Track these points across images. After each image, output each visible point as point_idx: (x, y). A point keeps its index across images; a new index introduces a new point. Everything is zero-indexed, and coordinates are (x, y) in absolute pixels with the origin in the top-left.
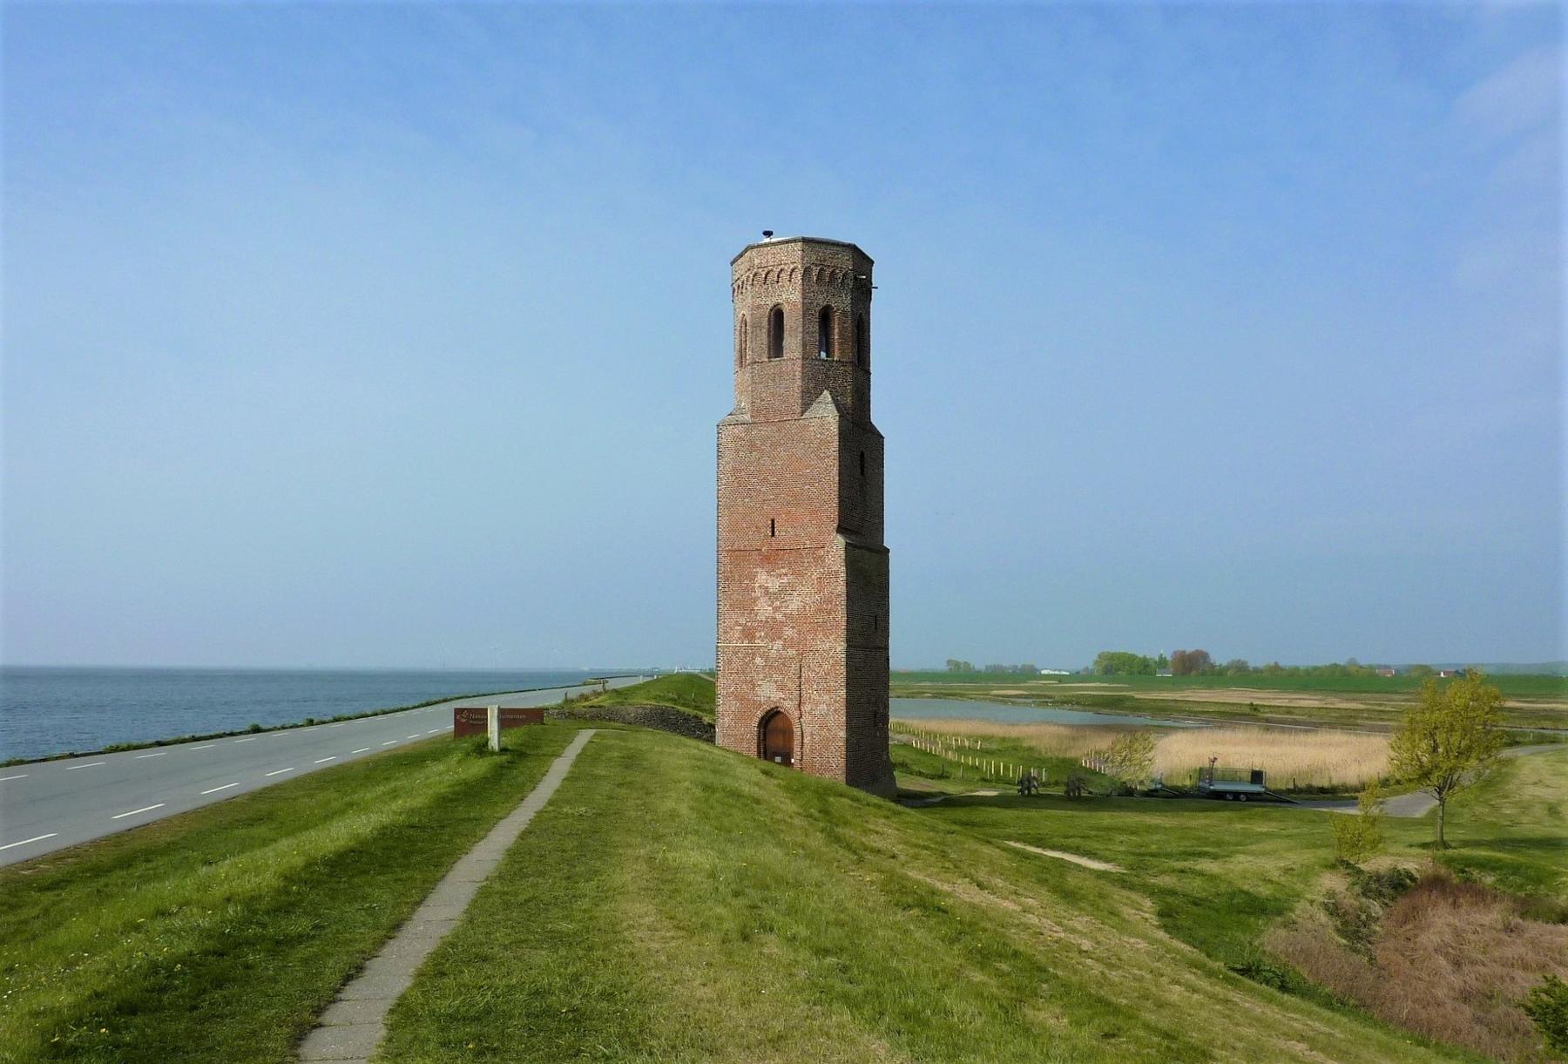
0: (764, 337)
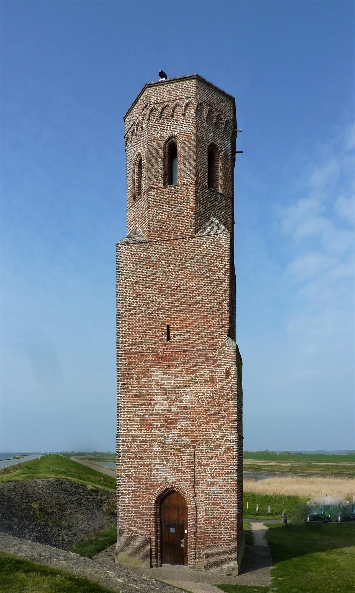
0: (159, 166)
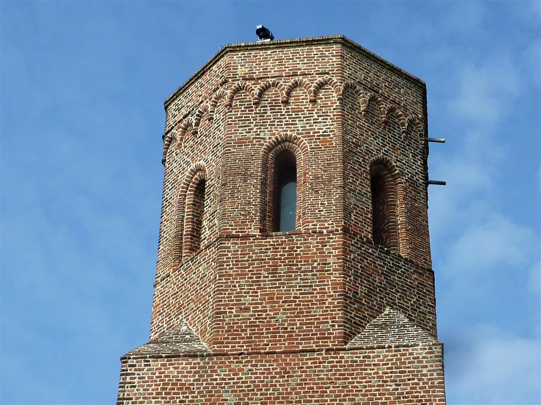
0: (253, 193)
